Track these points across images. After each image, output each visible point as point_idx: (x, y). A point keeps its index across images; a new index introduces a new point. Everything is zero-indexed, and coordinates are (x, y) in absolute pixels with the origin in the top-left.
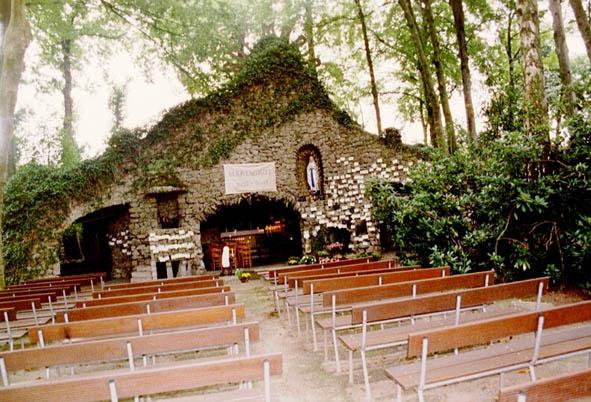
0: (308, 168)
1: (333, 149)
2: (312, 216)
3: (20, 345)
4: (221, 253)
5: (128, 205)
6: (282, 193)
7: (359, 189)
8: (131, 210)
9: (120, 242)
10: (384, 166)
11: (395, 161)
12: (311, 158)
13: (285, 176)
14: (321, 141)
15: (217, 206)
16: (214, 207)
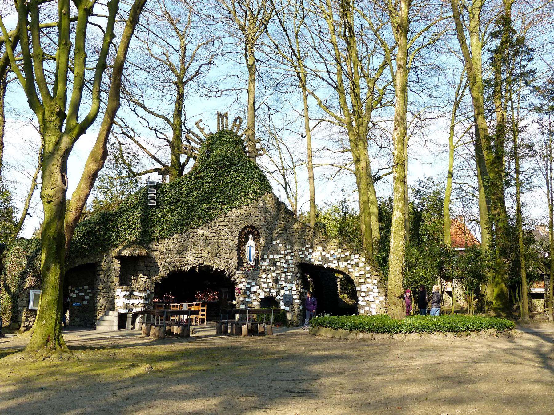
9: (82, 294)
12: (251, 237)
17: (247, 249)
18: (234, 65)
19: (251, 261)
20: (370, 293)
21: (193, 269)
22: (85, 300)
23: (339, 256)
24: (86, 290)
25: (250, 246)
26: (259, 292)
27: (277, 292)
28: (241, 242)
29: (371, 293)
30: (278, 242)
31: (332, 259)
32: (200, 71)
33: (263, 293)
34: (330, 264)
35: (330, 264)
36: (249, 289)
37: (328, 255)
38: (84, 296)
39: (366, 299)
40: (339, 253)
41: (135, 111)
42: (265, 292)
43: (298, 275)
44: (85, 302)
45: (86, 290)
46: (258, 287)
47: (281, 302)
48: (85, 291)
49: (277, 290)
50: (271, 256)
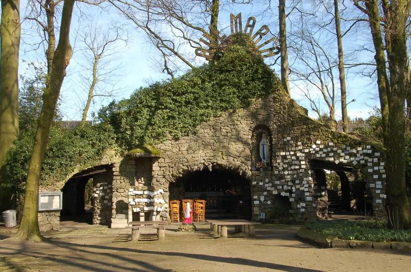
0: (260, 144)
19: (264, 158)
22: (106, 199)
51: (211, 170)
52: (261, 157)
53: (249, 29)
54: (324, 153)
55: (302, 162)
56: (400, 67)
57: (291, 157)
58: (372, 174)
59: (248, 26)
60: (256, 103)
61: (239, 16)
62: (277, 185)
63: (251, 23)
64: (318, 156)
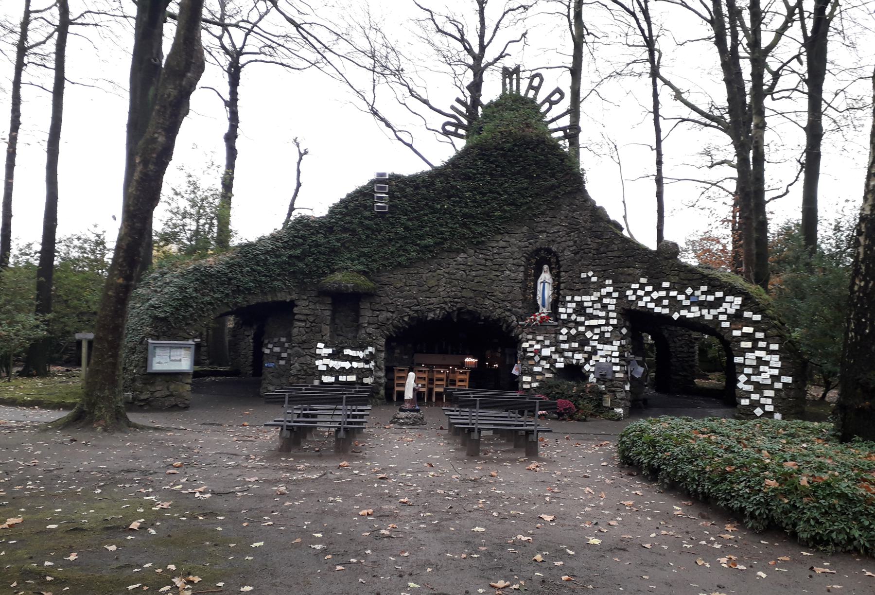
0: (539, 281)
1: (578, 257)
2: (77, 515)
3: (341, 399)
4: (405, 378)
5: (292, 304)
6: (499, 311)
7: (607, 318)
8: (296, 310)
9: (277, 349)
10: (649, 288)
11: (666, 284)
12: (546, 267)
13: (507, 290)
14: (564, 245)
15: (411, 318)
16: (406, 319)
17: (540, 287)
18: (703, 193)
19: (544, 306)
20: (762, 368)
21: (448, 317)
22: (282, 359)
23: (702, 298)
24: (284, 343)
25: (544, 282)
26: (555, 356)
27: (585, 358)
28: (530, 276)
29: (766, 368)
30: (590, 274)
31: (687, 303)
32: (506, 52)
33: (562, 359)
34: (684, 313)
35: (684, 313)
36: (787, 443)
37: (681, 297)
38: (280, 353)
39: (754, 378)
40: (703, 293)
41: (405, 104)
42: (566, 358)
43: (624, 331)
44: (282, 362)
45: (284, 343)
46: (553, 349)
47: (592, 376)
48: (281, 345)
49: (586, 356)
50: (577, 298)
51: (455, 320)
52: (540, 302)
53: (547, 105)
54: (652, 300)
55: (610, 313)
56: (386, 335)
57: (593, 304)
58: (739, 339)
59: (548, 100)
60: (63, 255)
61: (517, 70)
62: (564, 350)
63: (556, 97)
64: (641, 304)
